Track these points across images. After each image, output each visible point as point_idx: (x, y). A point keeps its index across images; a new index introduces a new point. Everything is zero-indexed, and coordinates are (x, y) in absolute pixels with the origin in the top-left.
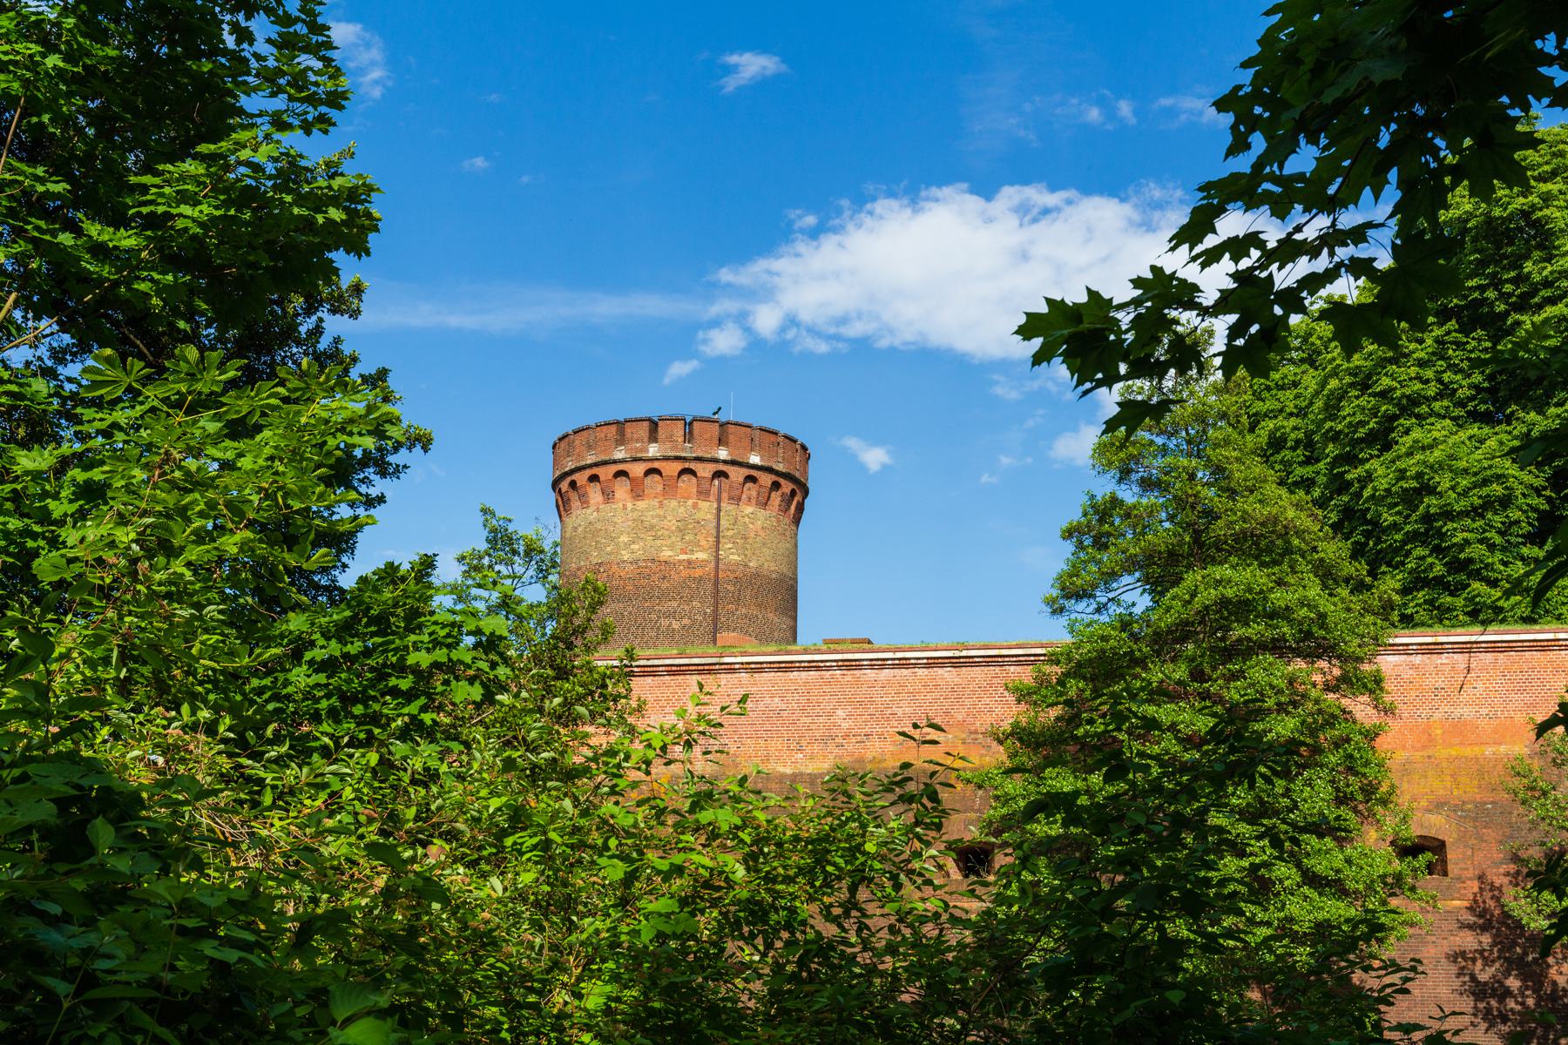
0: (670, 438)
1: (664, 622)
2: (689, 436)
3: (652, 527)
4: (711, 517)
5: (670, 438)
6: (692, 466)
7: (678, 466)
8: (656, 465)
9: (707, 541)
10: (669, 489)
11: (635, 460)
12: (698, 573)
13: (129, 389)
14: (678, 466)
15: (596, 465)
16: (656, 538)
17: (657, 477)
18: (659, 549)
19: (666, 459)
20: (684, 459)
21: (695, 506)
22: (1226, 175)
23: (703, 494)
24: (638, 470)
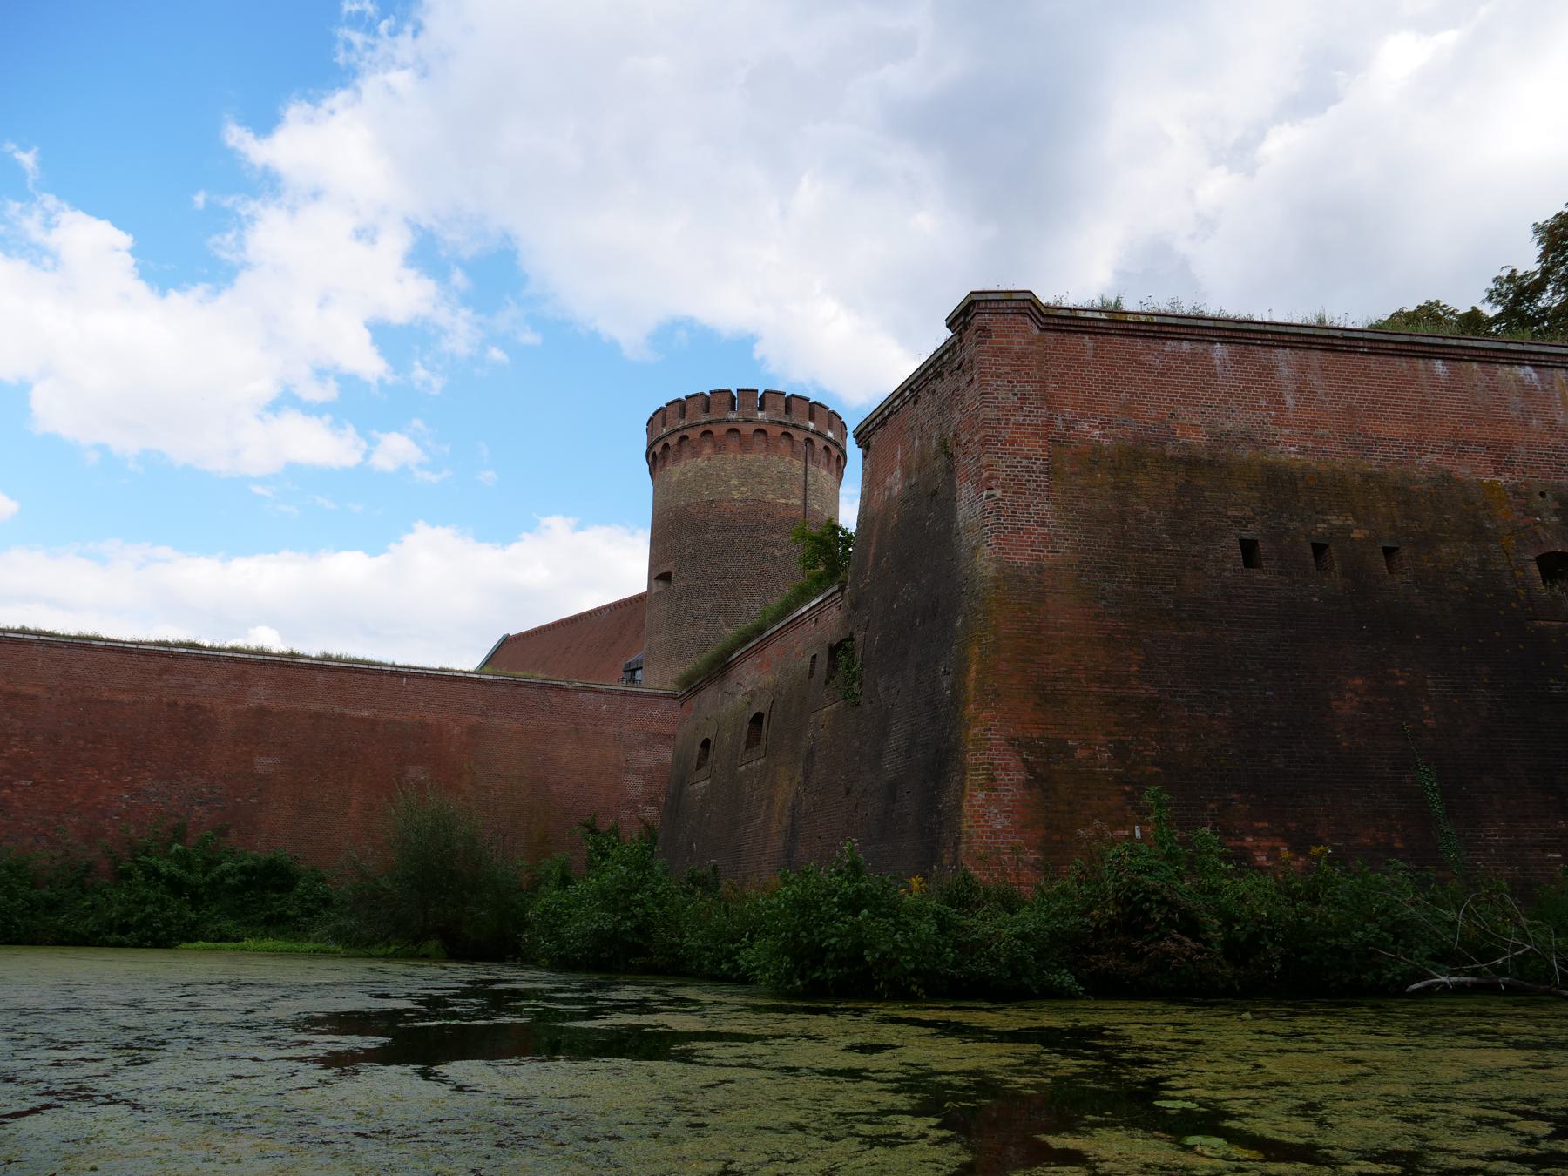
0: (774, 407)
1: (769, 550)
2: (788, 409)
3: (758, 475)
4: (801, 472)
5: (774, 407)
6: (790, 431)
7: (781, 430)
8: (763, 427)
9: (799, 492)
10: (770, 446)
11: (692, 426)
12: (794, 514)
13: (1315, 900)
14: (781, 430)
15: (684, 428)
16: (761, 483)
17: (762, 437)
18: (764, 492)
19: (772, 422)
20: (785, 425)
21: (791, 462)
22: (73, 631)
23: (795, 454)
24: (748, 429)
